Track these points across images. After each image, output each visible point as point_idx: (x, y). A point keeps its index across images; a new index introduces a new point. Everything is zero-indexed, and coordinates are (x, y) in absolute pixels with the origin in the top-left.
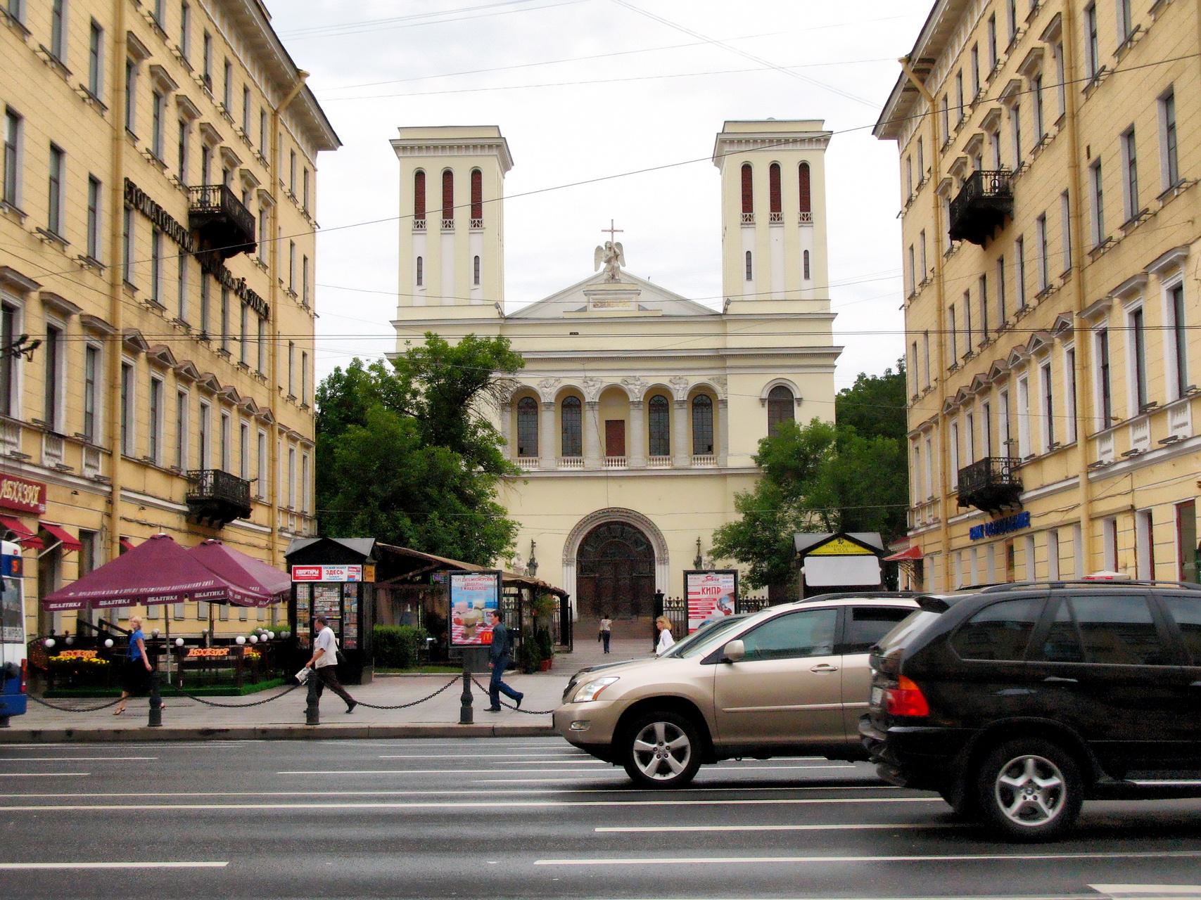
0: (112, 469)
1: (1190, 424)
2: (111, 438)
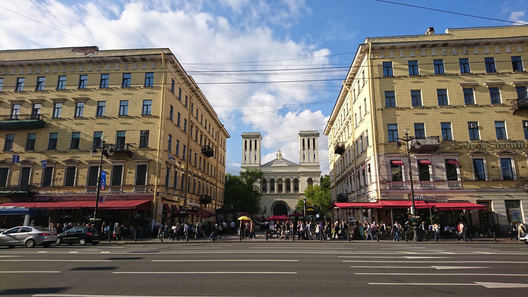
2: (186, 190)
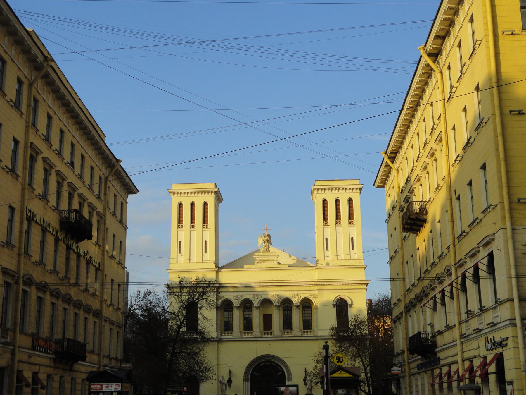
0: (14, 339)
1: (499, 316)
2: (15, 324)
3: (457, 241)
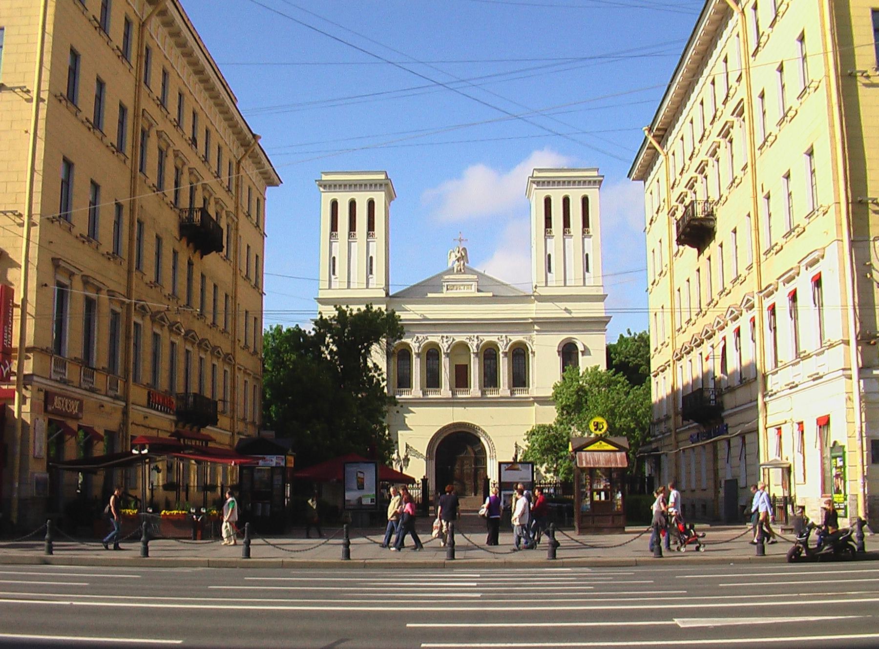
2: (126, 370)
3: (763, 258)
